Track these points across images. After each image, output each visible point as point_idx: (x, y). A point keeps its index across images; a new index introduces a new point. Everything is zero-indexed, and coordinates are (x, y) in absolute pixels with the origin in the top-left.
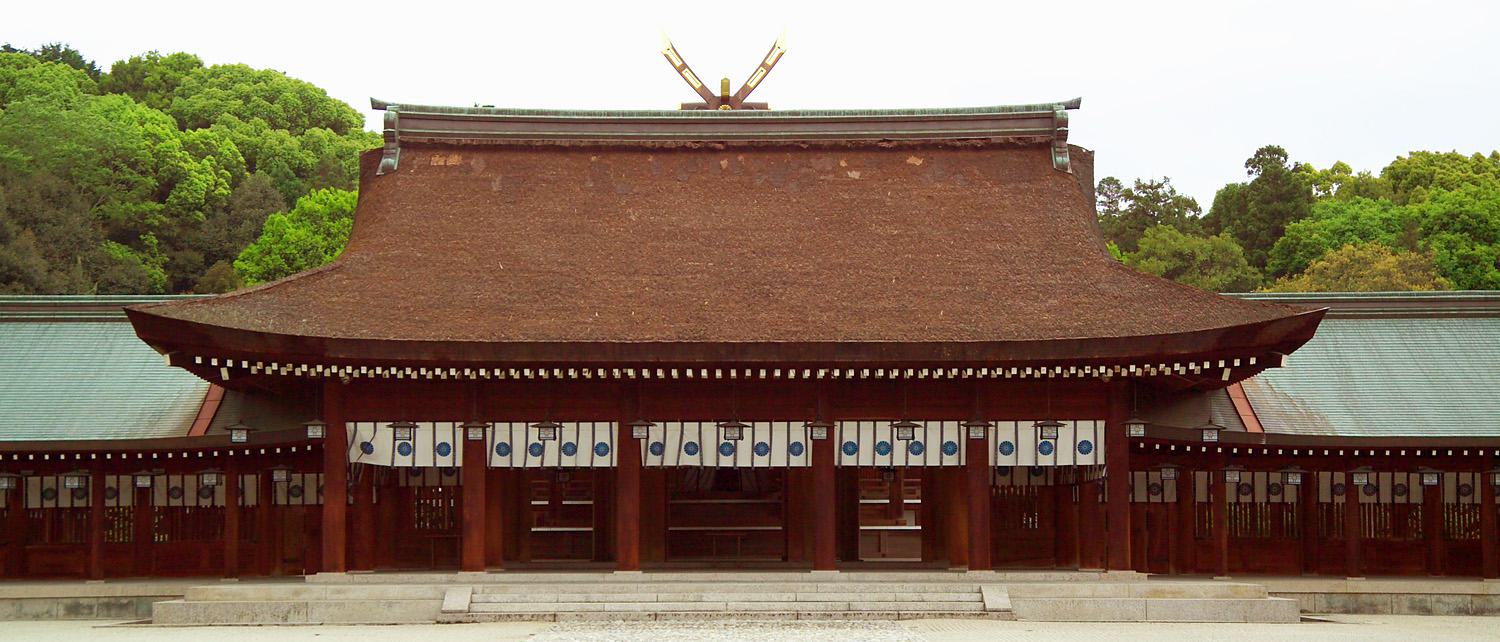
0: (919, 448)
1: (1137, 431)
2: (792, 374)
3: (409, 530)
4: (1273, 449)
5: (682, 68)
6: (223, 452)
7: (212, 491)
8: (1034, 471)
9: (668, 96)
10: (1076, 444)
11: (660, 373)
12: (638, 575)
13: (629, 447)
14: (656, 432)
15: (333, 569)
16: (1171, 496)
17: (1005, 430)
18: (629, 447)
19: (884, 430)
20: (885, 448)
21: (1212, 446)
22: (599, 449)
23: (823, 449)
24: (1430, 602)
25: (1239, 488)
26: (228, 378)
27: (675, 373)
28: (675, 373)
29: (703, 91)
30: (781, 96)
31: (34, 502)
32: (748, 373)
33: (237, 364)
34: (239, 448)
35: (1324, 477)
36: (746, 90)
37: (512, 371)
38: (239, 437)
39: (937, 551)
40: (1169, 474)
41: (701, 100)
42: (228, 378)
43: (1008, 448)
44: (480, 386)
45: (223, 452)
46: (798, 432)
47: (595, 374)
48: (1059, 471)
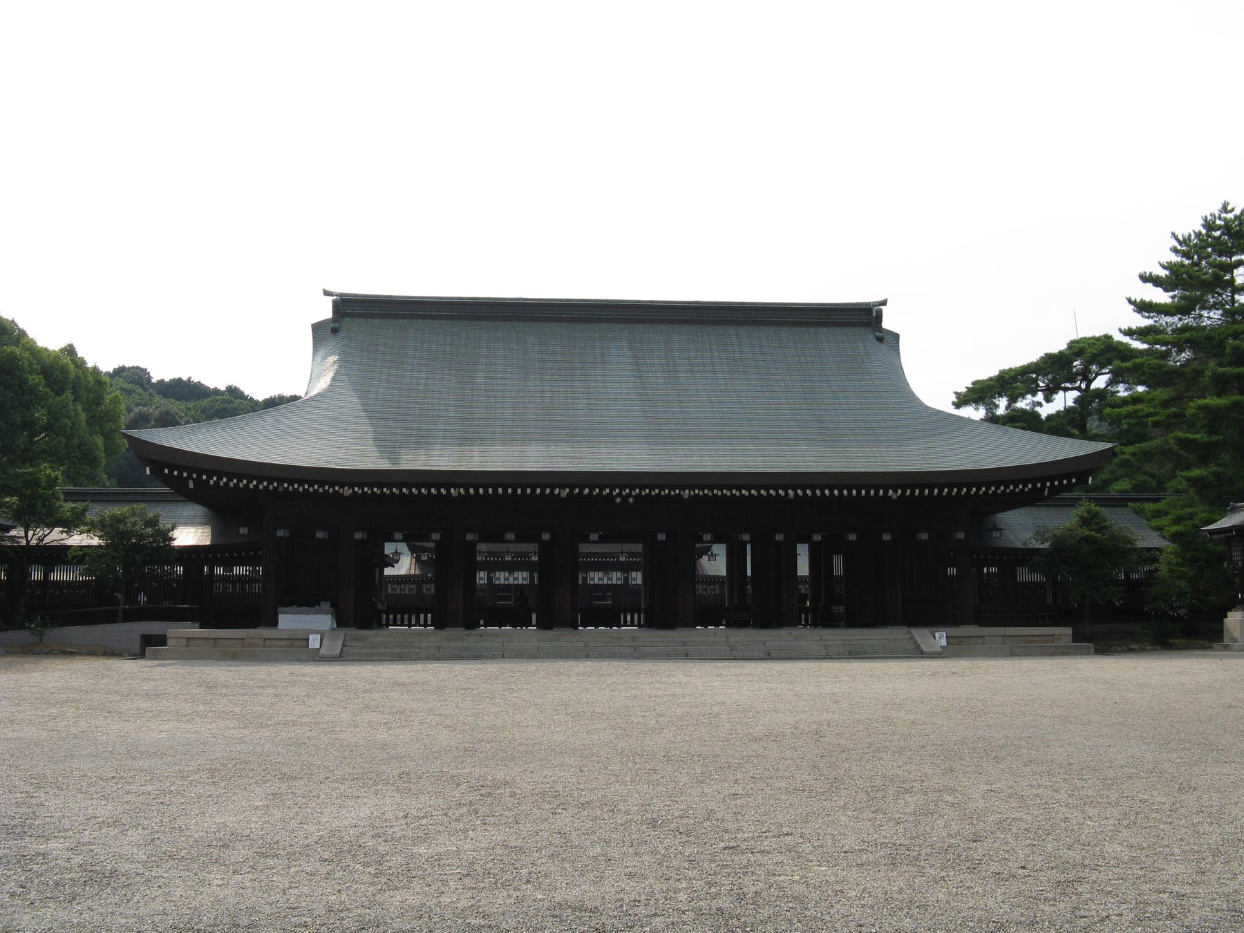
0: (610, 579)
2: (548, 491)
11: (818, 492)
14: (497, 574)
17: (634, 574)
19: (601, 574)
20: (506, 579)
22: (524, 579)
23: (626, 579)
26: (799, 546)
27: (836, 492)
28: (836, 492)
32: (529, 491)
33: (200, 476)
37: (433, 490)
42: (799, 546)
43: (635, 579)
46: (619, 574)
47: (439, 491)
48: (518, 585)
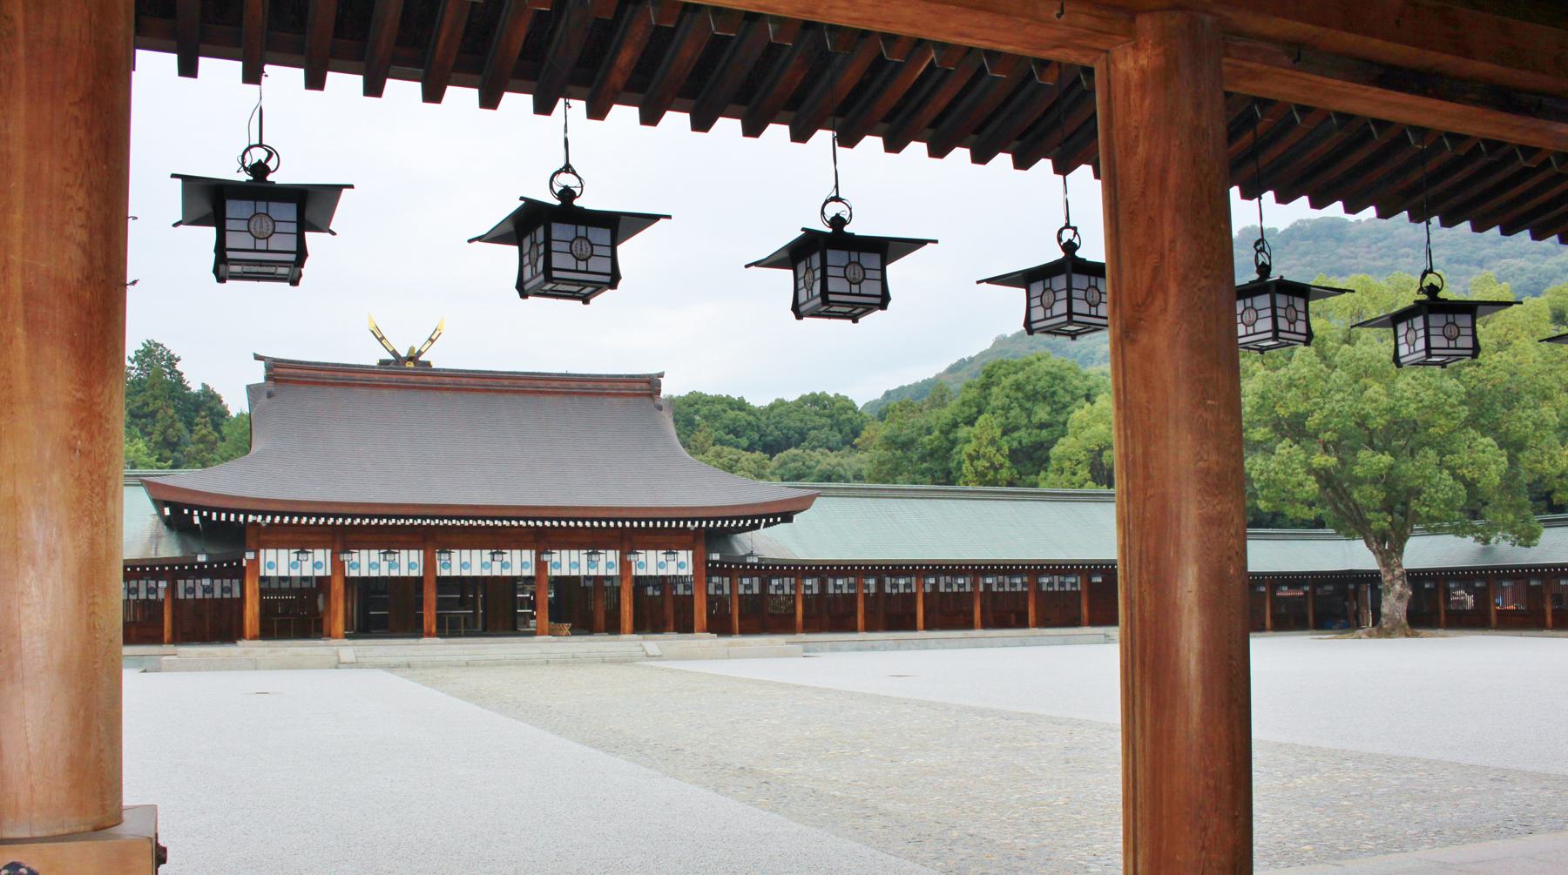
1: (716, 557)
3: (295, 615)
4: (759, 565)
5: (381, 339)
6: (191, 566)
7: (811, 587)
8: (587, 578)
9: (371, 355)
10: (680, 564)
12: (675, 635)
13: (541, 566)
14: (355, 557)
15: (429, 635)
16: (756, 590)
18: (541, 566)
20: (660, 565)
21: (752, 565)
24: (876, 644)
25: (906, 586)
29: (394, 353)
30: (440, 358)
31: (888, 590)
34: (201, 564)
35: (181, 583)
36: (420, 353)
38: (202, 558)
39: (449, 628)
40: (163, 584)
41: (391, 357)
44: (343, 530)
45: (191, 566)
